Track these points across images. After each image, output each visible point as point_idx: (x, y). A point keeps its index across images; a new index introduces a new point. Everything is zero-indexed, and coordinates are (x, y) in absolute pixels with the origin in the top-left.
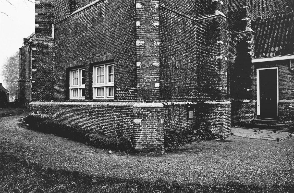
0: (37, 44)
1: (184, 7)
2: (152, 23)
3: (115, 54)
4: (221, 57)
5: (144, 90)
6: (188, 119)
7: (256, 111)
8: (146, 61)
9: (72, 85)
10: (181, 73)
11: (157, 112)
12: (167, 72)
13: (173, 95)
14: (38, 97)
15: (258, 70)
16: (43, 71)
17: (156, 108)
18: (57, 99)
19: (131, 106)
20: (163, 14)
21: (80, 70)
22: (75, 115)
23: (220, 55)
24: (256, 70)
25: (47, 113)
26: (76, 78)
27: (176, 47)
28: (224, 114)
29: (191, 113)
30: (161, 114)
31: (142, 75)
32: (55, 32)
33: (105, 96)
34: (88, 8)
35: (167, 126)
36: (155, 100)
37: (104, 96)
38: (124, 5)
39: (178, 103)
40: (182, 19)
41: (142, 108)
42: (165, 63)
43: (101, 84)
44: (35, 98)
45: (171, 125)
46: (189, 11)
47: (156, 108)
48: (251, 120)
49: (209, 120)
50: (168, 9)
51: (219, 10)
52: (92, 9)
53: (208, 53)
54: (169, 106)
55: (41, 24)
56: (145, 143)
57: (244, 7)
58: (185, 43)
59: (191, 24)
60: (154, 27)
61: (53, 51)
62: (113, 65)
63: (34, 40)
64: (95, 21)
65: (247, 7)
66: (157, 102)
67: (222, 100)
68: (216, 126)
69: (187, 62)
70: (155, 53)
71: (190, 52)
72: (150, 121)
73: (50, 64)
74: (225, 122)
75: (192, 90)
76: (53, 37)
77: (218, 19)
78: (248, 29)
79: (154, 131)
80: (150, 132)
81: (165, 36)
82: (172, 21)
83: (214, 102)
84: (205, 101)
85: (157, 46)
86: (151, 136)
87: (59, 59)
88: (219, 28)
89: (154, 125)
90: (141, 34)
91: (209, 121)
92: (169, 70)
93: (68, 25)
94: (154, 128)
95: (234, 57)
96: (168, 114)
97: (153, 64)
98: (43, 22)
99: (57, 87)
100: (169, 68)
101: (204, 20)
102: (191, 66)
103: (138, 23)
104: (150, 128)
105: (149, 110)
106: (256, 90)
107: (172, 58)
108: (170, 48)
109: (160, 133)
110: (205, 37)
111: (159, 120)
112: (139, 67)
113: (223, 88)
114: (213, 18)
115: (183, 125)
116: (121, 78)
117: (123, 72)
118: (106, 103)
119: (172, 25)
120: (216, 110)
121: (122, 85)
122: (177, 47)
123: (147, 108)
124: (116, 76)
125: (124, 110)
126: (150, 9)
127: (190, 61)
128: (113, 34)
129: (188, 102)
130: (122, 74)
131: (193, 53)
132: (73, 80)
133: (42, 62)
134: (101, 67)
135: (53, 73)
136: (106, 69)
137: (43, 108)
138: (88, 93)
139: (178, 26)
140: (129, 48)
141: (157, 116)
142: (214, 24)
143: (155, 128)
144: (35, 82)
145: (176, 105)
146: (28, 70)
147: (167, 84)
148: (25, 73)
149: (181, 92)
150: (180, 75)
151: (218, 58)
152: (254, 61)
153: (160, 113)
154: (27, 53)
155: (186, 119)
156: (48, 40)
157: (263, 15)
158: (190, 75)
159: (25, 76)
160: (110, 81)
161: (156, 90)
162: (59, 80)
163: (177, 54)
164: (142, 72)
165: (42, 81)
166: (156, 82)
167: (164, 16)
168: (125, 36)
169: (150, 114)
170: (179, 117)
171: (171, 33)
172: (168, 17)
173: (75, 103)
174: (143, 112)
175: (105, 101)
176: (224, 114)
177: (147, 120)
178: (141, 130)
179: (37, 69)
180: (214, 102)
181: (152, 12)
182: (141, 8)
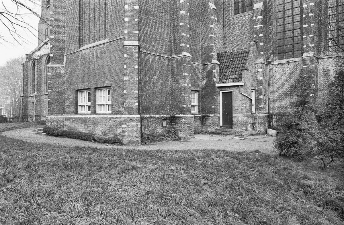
0: (52, 70)
3: (112, 82)
4: (186, 85)
5: (128, 107)
7: (219, 123)
9: (80, 103)
14: (53, 112)
15: (221, 92)
16: (56, 91)
18: (68, 113)
20: (144, 56)
21: (87, 91)
22: (83, 125)
23: (184, 83)
24: (220, 92)
25: (60, 124)
26: (84, 97)
29: (165, 124)
32: (66, 61)
33: (105, 111)
34: (93, 47)
37: (104, 111)
38: (118, 50)
39: (154, 116)
40: (159, 58)
43: (102, 102)
44: (50, 112)
45: (149, 130)
50: (148, 53)
51: (185, 51)
52: (96, 48)
53: (177, 82)
54: (148, 117)
55: (55, 54)
56: (129, 139)
57: (211, 45)
58: (161, 74)
59: (166, 61)
60: (135, 69)
61: (65, 75)
62: (111, 89)
63: (49, 67)
64: (98, 57)
65: (213, 45)
66: (136, 115)
67: (186, 114)
68: (182, 132)
69: (163, 87)
71: (165, 80)
73: (62, 86)
74: (188, 129)
75: (167, 107)
76: (64, 65)
77: (184, 59)
78: (213, 61)
81: (145, 71)
83: (181, 115)
87: (70, 82)
88: (184, 64)
91: (177, 129)
93: (77, 57)
95: (204, 82)
96: (147, 123)
97: (134, 91)
98: (57, 52)
99: (68, 104)
100: (148, 92)
103: (125, 67)
109: (138, 133)
111: (137, 126)
112: (126, 93)
114: (181, 57)
115: (158, 131)
116: (116, 98)
117: (117, 95)
118: (106, 116)
119: (151, 63)
120: (182, 121)
121: (117, 103)
123: (130, 118)
124: (112, 97)
125: (118, 120)
126: (132, 58)
127: (165, 87)
128: (111, 68)
129: (163, 115)
130: (117, 96)
132: (81, 98)
133: (56, 84)
134: (103, 90)
135: (65, 93)
136: (105, 92)
137: (58, 121)
138: (92, 108)
140: (121, 79)
141: (137, 123)
143: (135, 130)
144: (50, 100)
145: (153, 117)
146: (31, 86)
147: (147, 103)
148: (28, 88)
149: (157, 109)
150: (157, 97)
151: (184, 85)
152: (217, 85)
154: (29, 68)
156: (61, 67)
157: (233, 47)
159: (27, 91)
160: (109, 100)
161: (136, 107)
162: (70, 99)
164: (127, 96)
165: (56, 99)
166: (136, 102)
168: (119, 71)
170: (155, 125)
173: (83, 116)
175: (105, 114)
177: (130, 125)
178: (126, 132)
179: (52, 90)
180: (181, 115)
182: (127, 57)
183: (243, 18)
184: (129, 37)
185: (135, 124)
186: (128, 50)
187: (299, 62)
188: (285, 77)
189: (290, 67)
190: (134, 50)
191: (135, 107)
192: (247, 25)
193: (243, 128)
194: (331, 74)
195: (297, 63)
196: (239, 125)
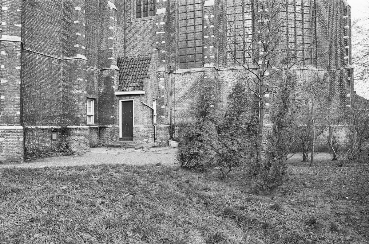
1: (50, 49)
2: (15, 67)
5: (7, 117)
6: (52, 140)
7: (119, 135)
8: (9, 95)
10: (45, 103)
11: (18, 133)
12: (31, 102)
13: (37, 121)
15: (120, 101)
17: (17, 130)
19: (187, 124)
27: (41, 82)
28: (81, 136)
30: (21, 134)
31: (5, 105)
35: (30, 145)
36: (16, 124)
39: (42, 127)
40: (48, 59)
41: (5, 130)
42: (30, 95)
45: (35, 144)
46: (56, 52)
47: (17, 130)
48: (113, 141)
49: (70, 141)
53: (71, 87)
54: (33, 129)
56: (7, 155)
57: (110, 48)
58: (50, 78)
59: (57, 63)
66: (17, 126)
67: (80, 125)
69: (52, 94)
70: (17, 89)
72: (11, 140)
75: (57, 116)
77: (78, 62)
79: (15, 147)
80: (11, 148)
82: (37, 61)
83: (74, 126)
84: (68, 126)
85: (18, 85)
86: (12, 151)
88: (79, 68)
89: (15, 143)
90: (5, 75)
91: (70, 142)
92: (34, 101)
94: (15, 145)
95: (102, 89)
96: (32, 136)
101: (68, 60)
102: (56, 97)
104: (11, 145)
105: (11, 132)
106: (119, 117)
107: (37, 91)
108: (35, 83)
110: (69, 74)
111: (19, 139)
112: (3, 99)
113: (82, 115)
120: (75, 132)
122: (42, 82)
127: (56, 93)
129: (52, 127)
131: (59, 86)
139: (44, 65)
142: (75, 66)
145: (40, 129)
147: (32, 111)
153: (20, 134)
155: (50, 140)
158: (55, 104)
161: (17, 116)
163: (42, 87)
164: (5, 103)
166: (17, 111)
167: (30, 57)
169: (11, 134)
171: (37, 71)
172: (33, 58)
174: (6, 133)
176: (81, 136)
178: (4, 146)
180: (74, 126)
181: (15, 59)
182: (6, 55)
183: (145, 23)
184: (8, 31)
185: (15, 137)
186: (7, 47)
187: (200, 73)
188: (187, 87)
189: (192, 77)
190: (16, 47)
191: (16, 116)
192: (150, 31)
193: (144, 140)
194: (229, 86)
195: (198, 73)
196: (139, 136)
